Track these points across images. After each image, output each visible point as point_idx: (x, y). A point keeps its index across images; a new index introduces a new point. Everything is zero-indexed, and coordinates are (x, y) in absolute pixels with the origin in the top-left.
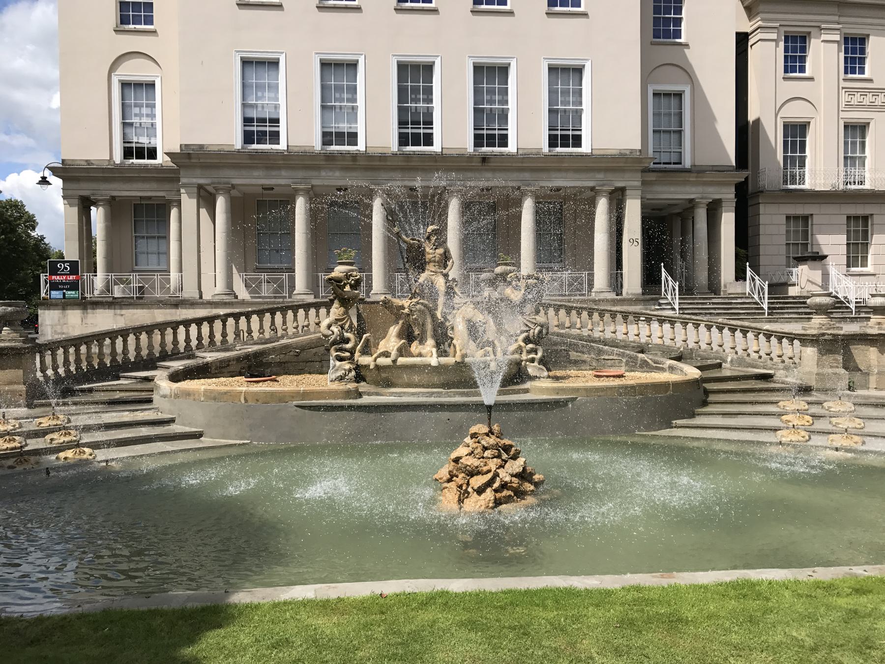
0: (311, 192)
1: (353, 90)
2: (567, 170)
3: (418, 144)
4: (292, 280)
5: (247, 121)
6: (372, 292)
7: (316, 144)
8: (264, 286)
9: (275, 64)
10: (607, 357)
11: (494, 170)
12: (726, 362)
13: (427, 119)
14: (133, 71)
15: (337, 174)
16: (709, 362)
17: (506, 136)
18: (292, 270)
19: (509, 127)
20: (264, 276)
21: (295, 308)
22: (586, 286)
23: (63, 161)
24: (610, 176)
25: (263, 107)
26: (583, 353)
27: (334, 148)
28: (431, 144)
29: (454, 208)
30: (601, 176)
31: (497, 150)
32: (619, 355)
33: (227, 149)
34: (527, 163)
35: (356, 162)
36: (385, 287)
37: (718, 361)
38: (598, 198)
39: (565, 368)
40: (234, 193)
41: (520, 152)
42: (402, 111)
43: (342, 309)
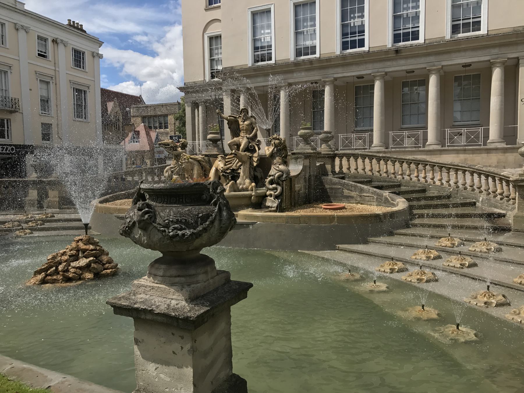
0: (441, 71)
1: (313, 19)
2: (465, 50)
3: (307, 54)
4: (371, 136)
5: (256, 49)
6: (427, 143)
7: (447, 35)
8: (406, 140)
9: (268, 11)
10: (365, 195)
11: (407, 57)
12: (478, 201)
13: (361, 29)
14: (213, 30)
15: (303, 74)
16: (468, 201)
17: (363, 40)
18: (372, 130)
19: (482, 15)
20: (406, 133)
21: (371, 158)
22: (368, 143)
23: (185, 83)
24: (504, 50)
25: (307, 32)
26: (351, 191)
27: (461, 35)
28: (363, 46)
29: (433, 81)
30: (495, 51)
31: (357, 50)
32: (372, 193)
33: (244, 67)
34: (379, 56)
35: (311, 66)
36: (437, 140)
37: (474, 200)
38: (493, 69)
39: (341, 201)
40: (387, 78)
41: (427, 42)
42: (344, 26)
43: (175, 161)
